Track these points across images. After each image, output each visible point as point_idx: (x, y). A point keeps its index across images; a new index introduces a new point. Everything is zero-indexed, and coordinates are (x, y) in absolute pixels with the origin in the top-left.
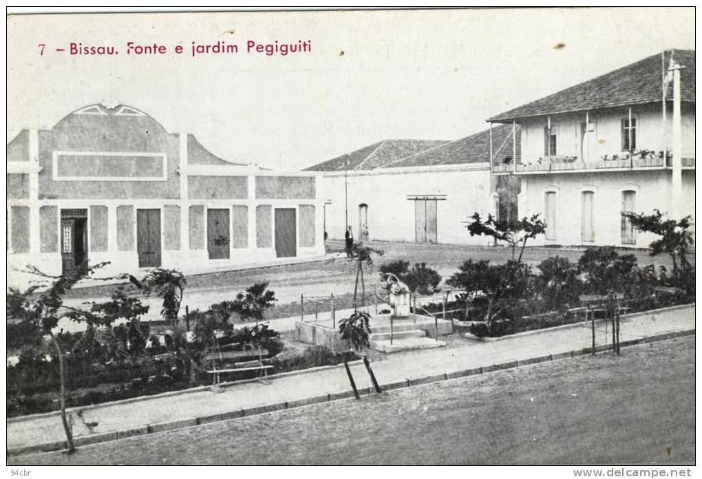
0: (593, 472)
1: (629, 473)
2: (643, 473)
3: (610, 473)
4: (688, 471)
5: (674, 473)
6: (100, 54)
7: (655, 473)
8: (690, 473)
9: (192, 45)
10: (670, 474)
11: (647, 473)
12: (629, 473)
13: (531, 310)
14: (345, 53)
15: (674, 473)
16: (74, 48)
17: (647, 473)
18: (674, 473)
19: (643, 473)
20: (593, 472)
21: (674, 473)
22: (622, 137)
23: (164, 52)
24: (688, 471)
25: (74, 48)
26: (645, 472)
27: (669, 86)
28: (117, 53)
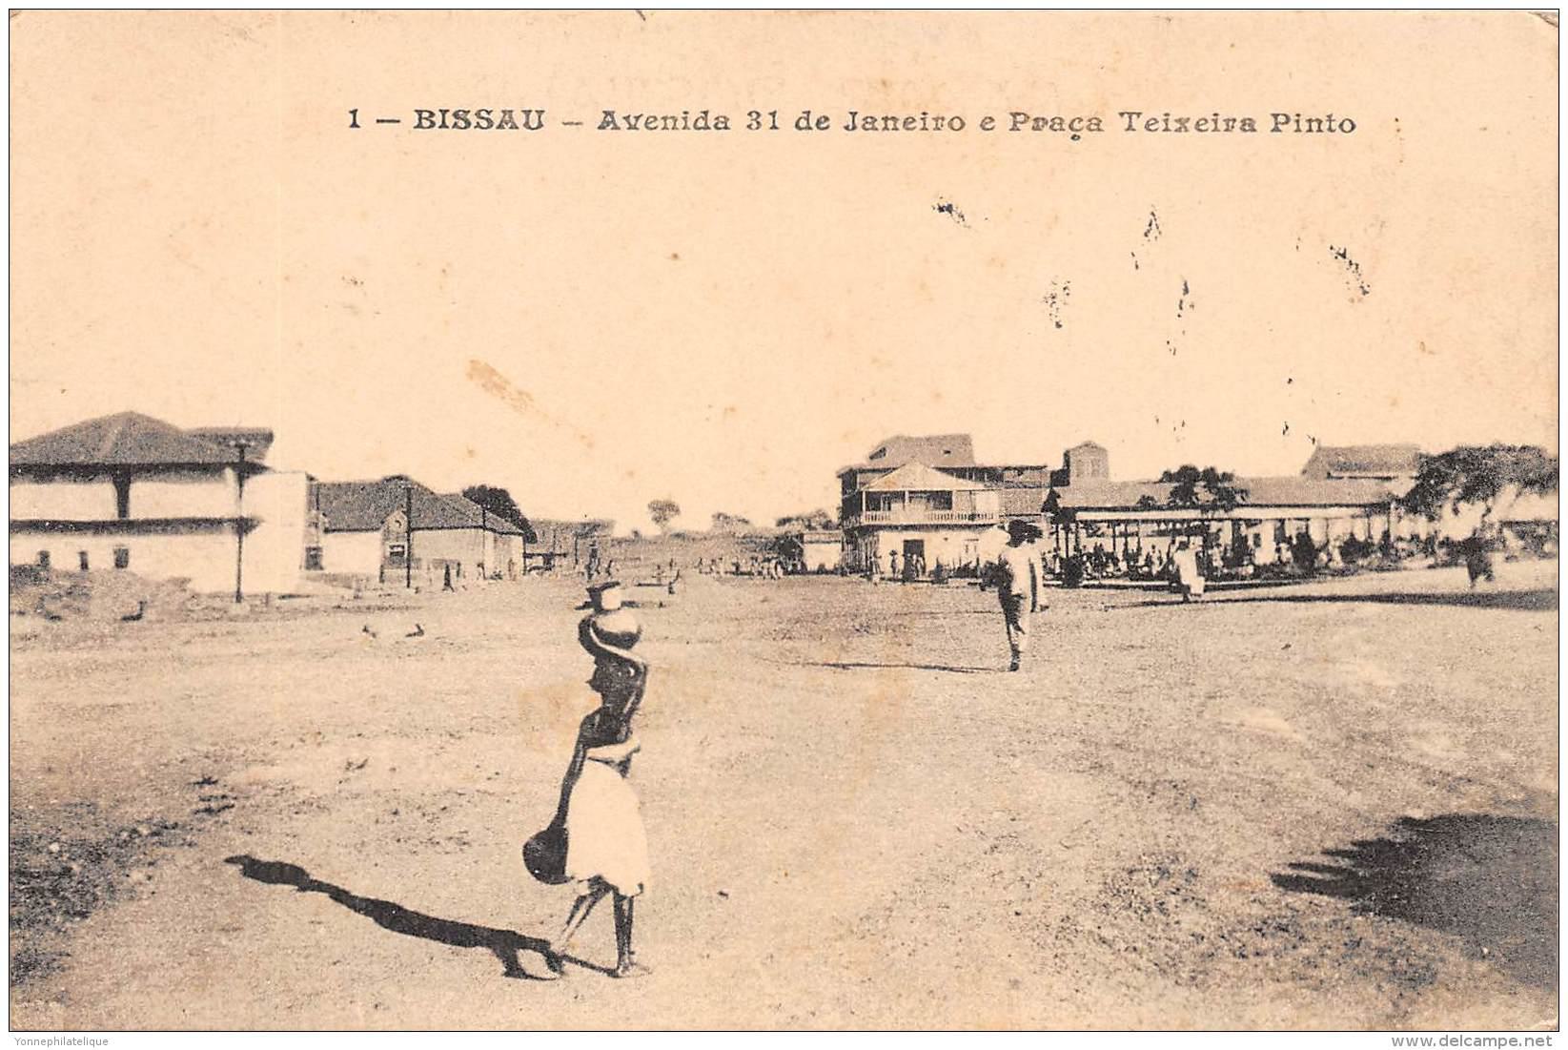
0: (1419, 1041)
1: (1468, 1042)
2: (1487, 1042)
3: (1444, 1042)
4: (1548, 1038)
5: (1529, 1042)
6: (953, 129)
7: (1502, 1042)
8: (1550, 1042)
9: (891, 558)
10: (1523, 1044)
11: (1493, 1042)
12: (1468, 1042)
13: (888, 913)
14: (1058, 330)
15: (1529, 1042)
16: (608, 121)
17: (1493, 1042)
18: (1529, 1042)
19: (1487, 1042)
20: (1419, 1041)
21: (1529, 1042)
22: (193, 480)
23: (827, 128)
24: (1548, 1038)
25: (608, 121)
26: (1490, 1040)
27: (964, 477)
28: (1192, 306)
